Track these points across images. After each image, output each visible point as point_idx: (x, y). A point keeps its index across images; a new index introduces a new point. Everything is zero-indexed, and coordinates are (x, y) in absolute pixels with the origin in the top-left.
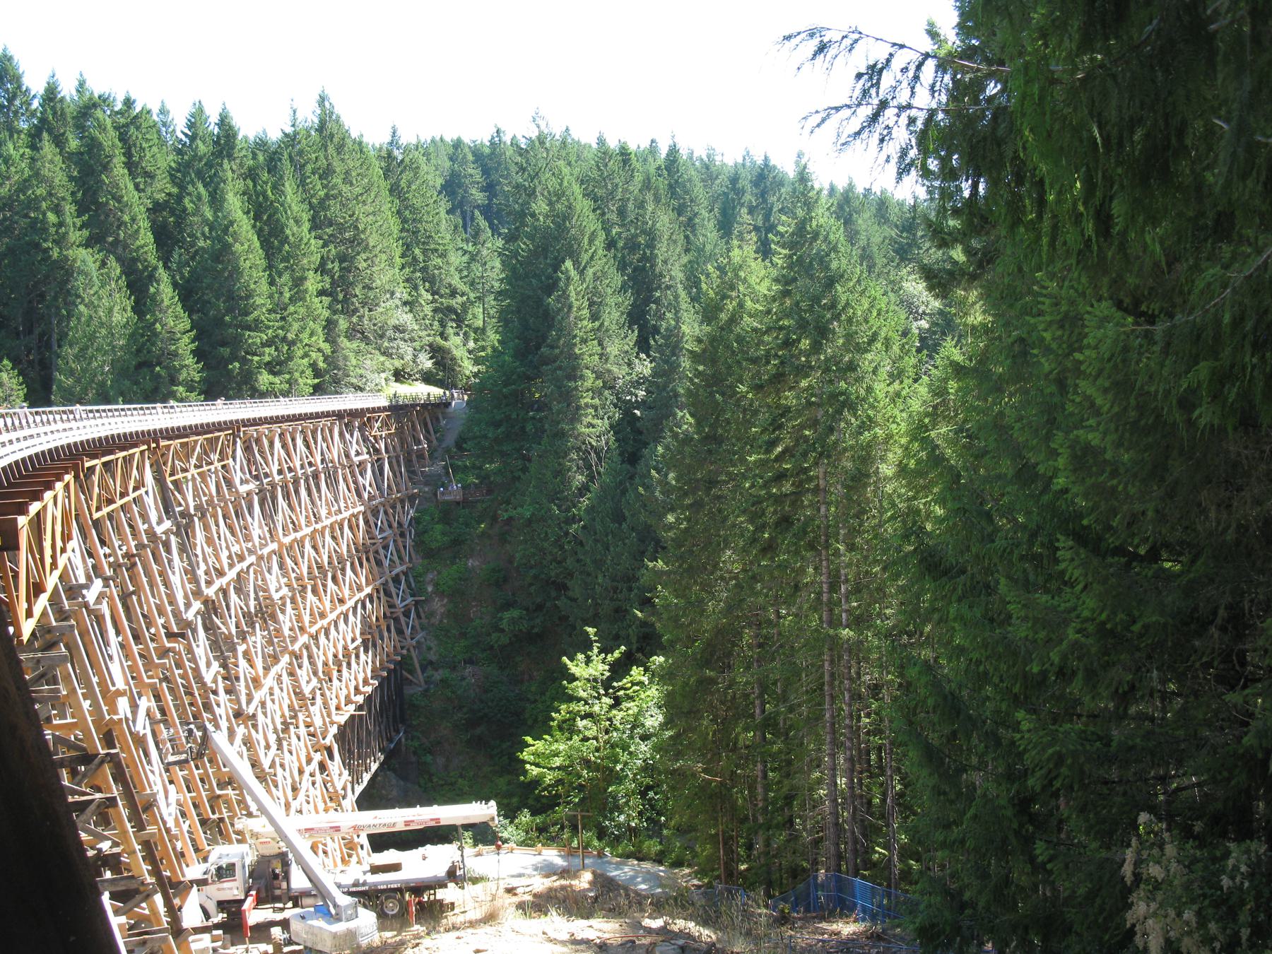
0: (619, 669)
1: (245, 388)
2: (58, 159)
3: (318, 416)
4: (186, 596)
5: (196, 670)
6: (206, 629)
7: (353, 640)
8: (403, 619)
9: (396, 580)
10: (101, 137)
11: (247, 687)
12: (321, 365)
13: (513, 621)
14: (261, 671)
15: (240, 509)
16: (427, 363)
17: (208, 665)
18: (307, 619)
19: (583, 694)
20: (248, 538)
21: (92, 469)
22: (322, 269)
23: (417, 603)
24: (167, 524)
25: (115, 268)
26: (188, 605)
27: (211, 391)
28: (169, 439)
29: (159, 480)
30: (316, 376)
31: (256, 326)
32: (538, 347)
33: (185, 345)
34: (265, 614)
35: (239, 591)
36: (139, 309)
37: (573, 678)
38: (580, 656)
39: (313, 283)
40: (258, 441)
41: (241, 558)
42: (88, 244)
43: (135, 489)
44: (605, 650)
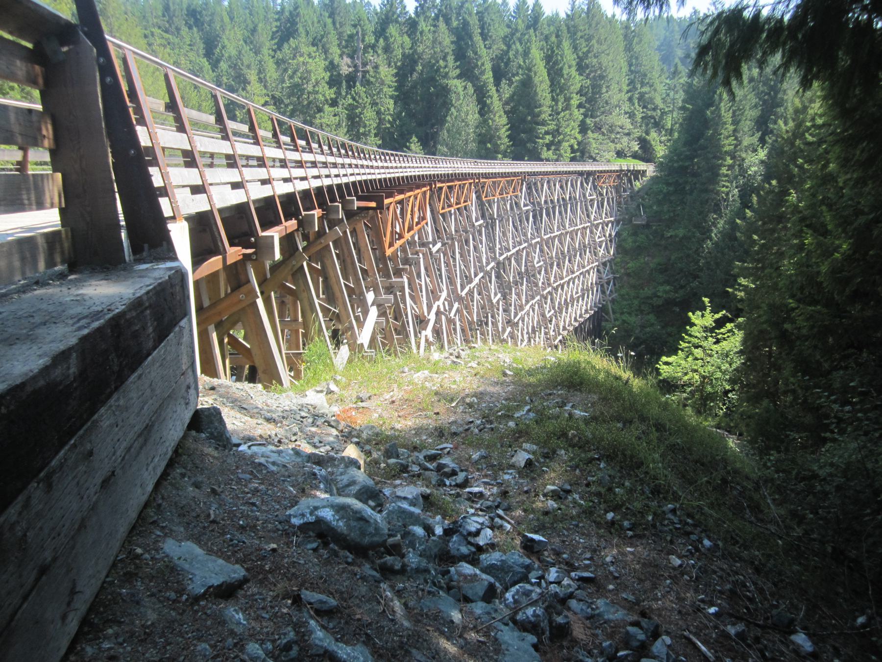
0: (720, 323)
1: (535, 157)
2: (447, 32)
3: (570, 173)
4: (487, 259)
5: (489, 296)
6: (497, 277)
7: (577, 293)
8: (606, 286)
9: (604, 264)
10: (469, 19)
11: (515, 309)
12: (576, 147)
13: (665, 292)
14: (524, 302)
15: (522, 218)
16: (636, 147)
17: (496, 294)
18: (552, 279)
19: (697, 334)
20: (525, 235)
21: (441, 188)
22: (580, 92)
23: (615, 278)
24: (481, 222)
25: (471, 90)
26: (488, 264)
27: (517, 157)
28: (487, 178)
29: (479, 197)
30: (572, 153)
31: (544, 123)
32: (698, 140)
33: (504, 133)
34: (530, 275)
35: (517, 261)
36: (482, 113)
37: (692, 325)
38: (699, 313)
39: (575, 101)
40: (535, 184)
41: (520, 244)
42: (459, 77)
43: (465, 202)
44: (715, 311)
